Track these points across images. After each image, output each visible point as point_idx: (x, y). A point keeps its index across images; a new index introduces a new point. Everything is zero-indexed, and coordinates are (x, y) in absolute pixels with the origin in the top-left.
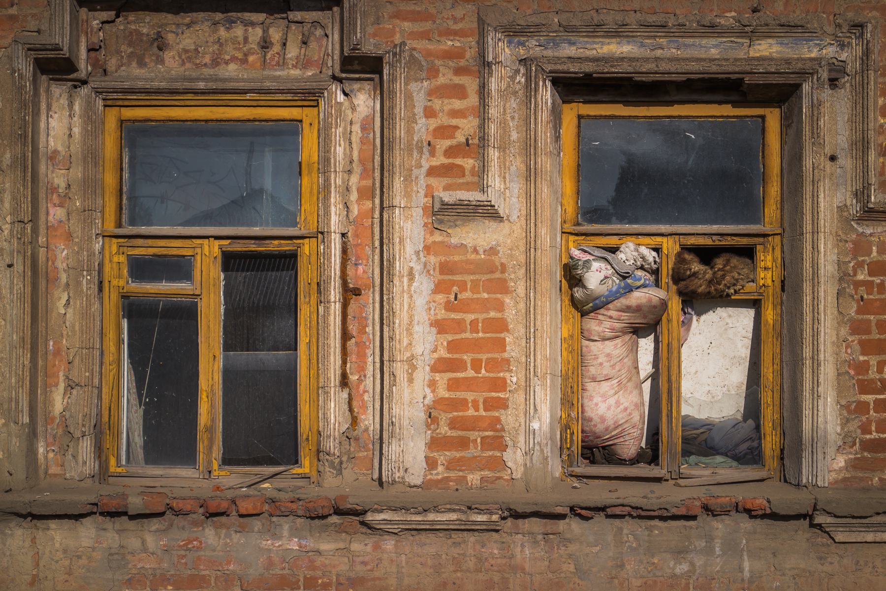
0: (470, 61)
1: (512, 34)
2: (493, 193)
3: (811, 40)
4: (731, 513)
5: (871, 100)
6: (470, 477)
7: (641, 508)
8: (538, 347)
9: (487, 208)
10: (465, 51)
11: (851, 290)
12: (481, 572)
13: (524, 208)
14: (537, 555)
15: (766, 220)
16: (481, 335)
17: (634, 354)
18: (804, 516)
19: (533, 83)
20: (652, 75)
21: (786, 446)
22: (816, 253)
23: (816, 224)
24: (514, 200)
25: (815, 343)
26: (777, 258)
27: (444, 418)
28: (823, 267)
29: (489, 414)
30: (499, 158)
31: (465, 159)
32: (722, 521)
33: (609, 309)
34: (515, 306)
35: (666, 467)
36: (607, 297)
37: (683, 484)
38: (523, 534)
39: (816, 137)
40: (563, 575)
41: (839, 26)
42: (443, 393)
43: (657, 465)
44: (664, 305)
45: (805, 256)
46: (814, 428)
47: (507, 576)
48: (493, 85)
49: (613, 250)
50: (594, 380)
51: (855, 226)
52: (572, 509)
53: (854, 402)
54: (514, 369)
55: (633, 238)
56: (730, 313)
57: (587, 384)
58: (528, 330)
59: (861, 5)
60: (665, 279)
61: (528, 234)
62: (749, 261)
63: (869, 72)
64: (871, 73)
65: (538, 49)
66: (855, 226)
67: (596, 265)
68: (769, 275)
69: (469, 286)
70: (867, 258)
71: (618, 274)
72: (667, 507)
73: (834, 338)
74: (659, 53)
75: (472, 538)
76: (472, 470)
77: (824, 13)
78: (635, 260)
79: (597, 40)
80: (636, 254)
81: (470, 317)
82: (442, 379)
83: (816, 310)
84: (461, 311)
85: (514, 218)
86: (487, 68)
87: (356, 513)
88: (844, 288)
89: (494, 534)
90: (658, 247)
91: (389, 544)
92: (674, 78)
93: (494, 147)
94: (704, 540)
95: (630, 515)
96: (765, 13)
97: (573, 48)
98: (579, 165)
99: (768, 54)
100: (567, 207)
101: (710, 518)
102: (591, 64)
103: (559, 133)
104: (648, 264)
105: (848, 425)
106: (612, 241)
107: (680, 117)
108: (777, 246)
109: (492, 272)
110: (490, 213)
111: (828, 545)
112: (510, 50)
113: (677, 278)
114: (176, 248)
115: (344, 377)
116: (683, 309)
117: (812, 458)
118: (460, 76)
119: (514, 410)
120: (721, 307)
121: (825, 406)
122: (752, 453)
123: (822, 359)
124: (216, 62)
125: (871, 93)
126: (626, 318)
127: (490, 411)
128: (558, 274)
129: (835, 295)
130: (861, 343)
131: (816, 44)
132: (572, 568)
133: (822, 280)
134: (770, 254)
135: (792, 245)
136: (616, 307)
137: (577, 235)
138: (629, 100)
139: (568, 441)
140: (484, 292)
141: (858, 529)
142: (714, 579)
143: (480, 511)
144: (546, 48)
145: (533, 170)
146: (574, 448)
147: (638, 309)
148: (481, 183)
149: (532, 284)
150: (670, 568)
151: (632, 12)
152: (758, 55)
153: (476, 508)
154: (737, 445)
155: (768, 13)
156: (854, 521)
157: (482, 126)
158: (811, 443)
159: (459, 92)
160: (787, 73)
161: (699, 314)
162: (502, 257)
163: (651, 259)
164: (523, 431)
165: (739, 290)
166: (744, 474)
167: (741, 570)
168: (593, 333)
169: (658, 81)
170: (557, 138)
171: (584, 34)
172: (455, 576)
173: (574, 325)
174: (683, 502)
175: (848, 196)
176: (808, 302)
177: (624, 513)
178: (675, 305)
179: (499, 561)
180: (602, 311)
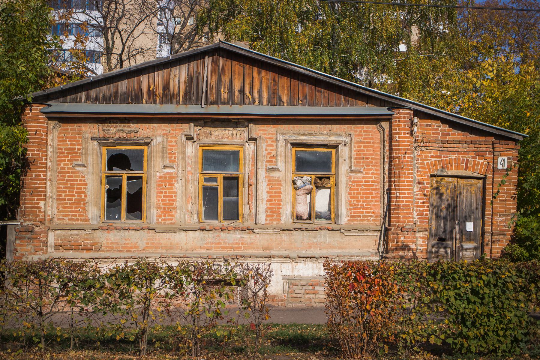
27: (269, 211)
42: (269, 206)
44: (312, 189)
81: (274, 191)
82: (268, 203)
87: (251, 230)
91: (258, 236)
106: (302, 176)
110: (279, 170)
113: (315, 183)
114: (213, 176)
115: (248, 202)
124: (222, 138)
147: (307, 189)
157: (277, 153)
159: (272, 146)
162: (281, 179)
178: (314, 188)
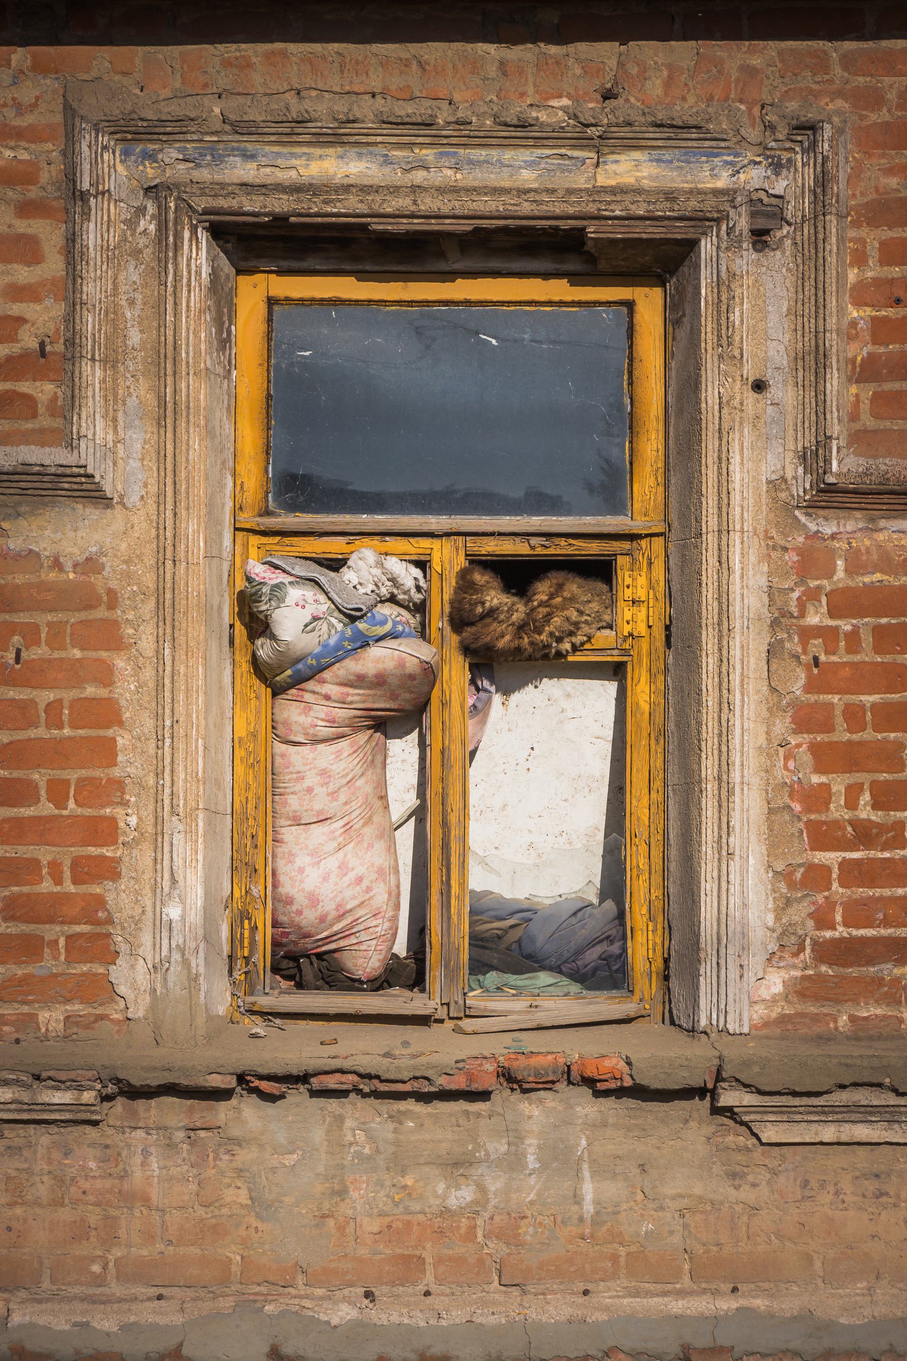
0: (49, 188)
1: (129, 136)
2: (91, 450)
3: (717, 155)
4: (558, 1086)
5: (832, 274)
6: (43, 1016)
7: (377, 1077)
8: (180, 756)
9: (78, 480)
10: (39, 169)
11: (794, 645)
12: (62, 1205)
13: (152, 481)
14: (174, 1171)
15: (636, 506)
16: (67, 731)
17: (379, 770)
18: (701, 1092)
19: (171, 233)
20: (405, 221)
21: (673, 953)
22: (726, 573)
23: (724, 515)
24: (134, 464)
25: (724, 749)
26: (658, 582)
28: (738, 599)
29: (84, 889)
30: (103, 381)
31: (38, 384)
32: (541, 1101)
33: (324, 682)
34: (136, 674)
35: (438, 995)
36: (318, 657)
37: (469, 1029)
38: (147, 1130)
39: (725, 345)
40: (225, 1211)
41: (770, 127)
43: (423, 990)
45: (704, 578)
46: (723, 918)
47: (113, 1212)
48: (91, 236)
49: (334, 564)
50: (297, 821)
51: (803, 519)
52: (241, 1078)
53: (800, 865)
54: (133, 799)
55: (375, 541)
56: (569, 689)
57: (283, 830)
58: (160, 723)
59: (815, 87)
60: (438, 622)
61: (161, 531)
62: (605, 587)
63: (828, 217)
64: (832, 220)
65: (182, 166)
66: (803, 519)
67: (295, 594)
68: (642, 615)
69: (43, 635)
70: (825, 582)
71: (340, 611)
72: (428, 1074)
73: (762, 740)
74: (419, 176)
75: (44, 1138)
76: (47, 1002)
77: (741, 101)
78: (376, 585)
79: (298, 150)
80: (377, 572)
81: (46, 696)
83: (725, 685)
84: (27, 684)
85: (133, 499)
86: (79, 203)
88: (781, 641)
89: (88, 1129)
90: (423, 558)
92: (448, 225)
93: (93, 359)
94: (504, 1141)
95: (359, 1091)
96: (627, 100)
97: (252, 166)
98: (269, 397)
99: (632, 181)
100: (245, 480)
101: (517, 1095)
102: (285, 197)
103: (229, 332)
104: (405, 593)
105: (790, 911)
106: (333, 547)
107: (468, 303)
108: (657, 557)
109: (90, 607)
111: (749, 1150)
112: (128, 168)
116: (473, 682)
117: (718, 977)
118: (28, 218)
119: (133, 882)
120: (551, 678)
121: (744, 872)
122: (608, 965)
123: (738, 780)
125: (832, 260)
126: (356, 698)
127: (84, 883)
128: (227, 612)
129: (764, 655)
130: (814, 748)
131: (727, 163)
132: (243, 1197)
133: (737, 624)
134: (643, 574)
135: (683, 556)
136: (337, 676)
137: (264, 533)
138: (368, 268)
139: (246, 944)
140: (74, 647)
141: (806, 1118)
142: (524, 1217)
143: (59, 1084)
144: (198, 166)
145: (170, 406)
146: (258, 958)
147: (379, 681)
148: (68, 431)
149: (169, 630)
150: (438, 1197)
151: (367, 97)
152: (613, 182)
153: (50, 1078)
154: (579, 952)
155: (632, 100)
156: (797, 1101)
157: (70, 319)
158: (715, 946)
160: (669, 218)
161: (507, 692)
163: (409, 583)
164: (150, 923)
165: (582, 644)
166: (593, 1008)
167: (577, 1199)
168: (295, 728)
169: (416, 232)
170: (224, 342)
171: (273, 138)
172: (10, 1213)
173: (258, 712)
174: (461, 1065)
175: (788, 461)
176: (710, 668)
177: (344, 1087)
179: (98, 1184)
180: (310, 685)
